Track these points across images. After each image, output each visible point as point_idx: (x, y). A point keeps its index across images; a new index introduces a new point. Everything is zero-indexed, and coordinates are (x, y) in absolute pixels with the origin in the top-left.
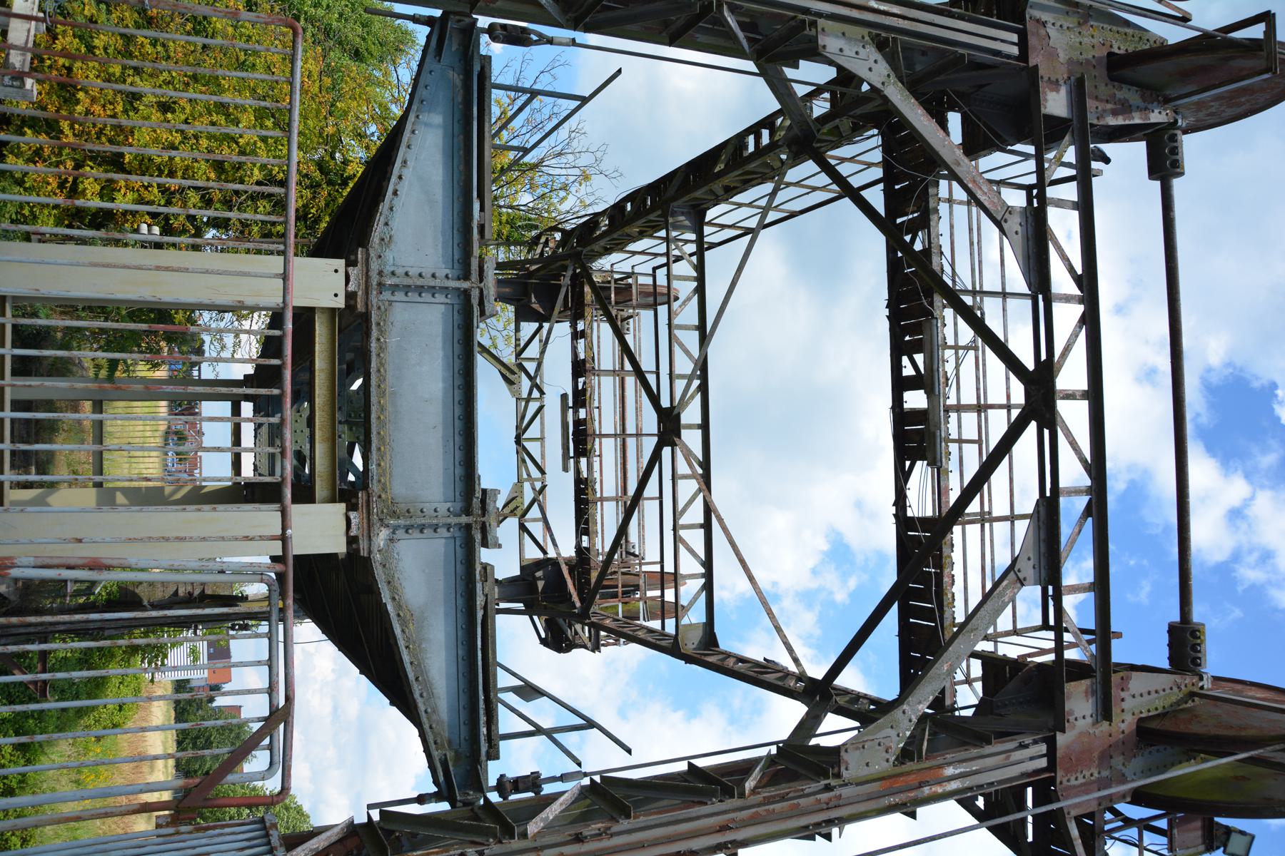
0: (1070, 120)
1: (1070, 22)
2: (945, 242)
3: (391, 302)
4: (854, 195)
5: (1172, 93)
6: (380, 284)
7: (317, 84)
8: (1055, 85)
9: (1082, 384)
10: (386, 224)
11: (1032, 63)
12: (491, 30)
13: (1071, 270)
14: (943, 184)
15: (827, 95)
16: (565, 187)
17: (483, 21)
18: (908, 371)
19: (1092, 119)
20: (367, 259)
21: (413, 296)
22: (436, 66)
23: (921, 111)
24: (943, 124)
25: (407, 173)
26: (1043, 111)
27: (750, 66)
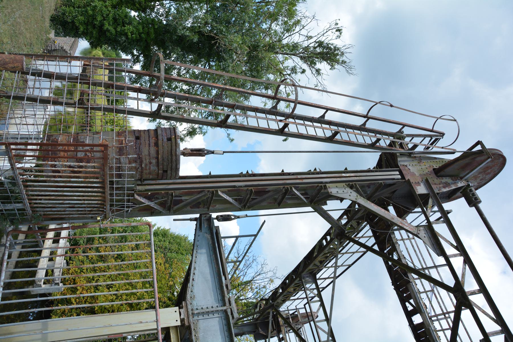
0: (429, 194)
1: (415, 163)
2: (405, 253)
3: (198, 320)
4: (370, 249)
5: (461, 175)
6: (193, 314)
7: (164, 267)
8: (418, 184)
9: (476, 287)
10: (192, 291)
11: (407, 179)
12: (217, 218)
13: (452, 245)
14: (397, 233)
15: (345, 217)
16: (264, 287)
17: (214, 215)
18: (410, 308)
19: (436, 191)
20: (186, 305)
21: (206, 316)
22: (200, 234)
23: (373, 205)
24: (388, 210)
25: (196, 272)
26: (417, 193)
27: (310, 209)
